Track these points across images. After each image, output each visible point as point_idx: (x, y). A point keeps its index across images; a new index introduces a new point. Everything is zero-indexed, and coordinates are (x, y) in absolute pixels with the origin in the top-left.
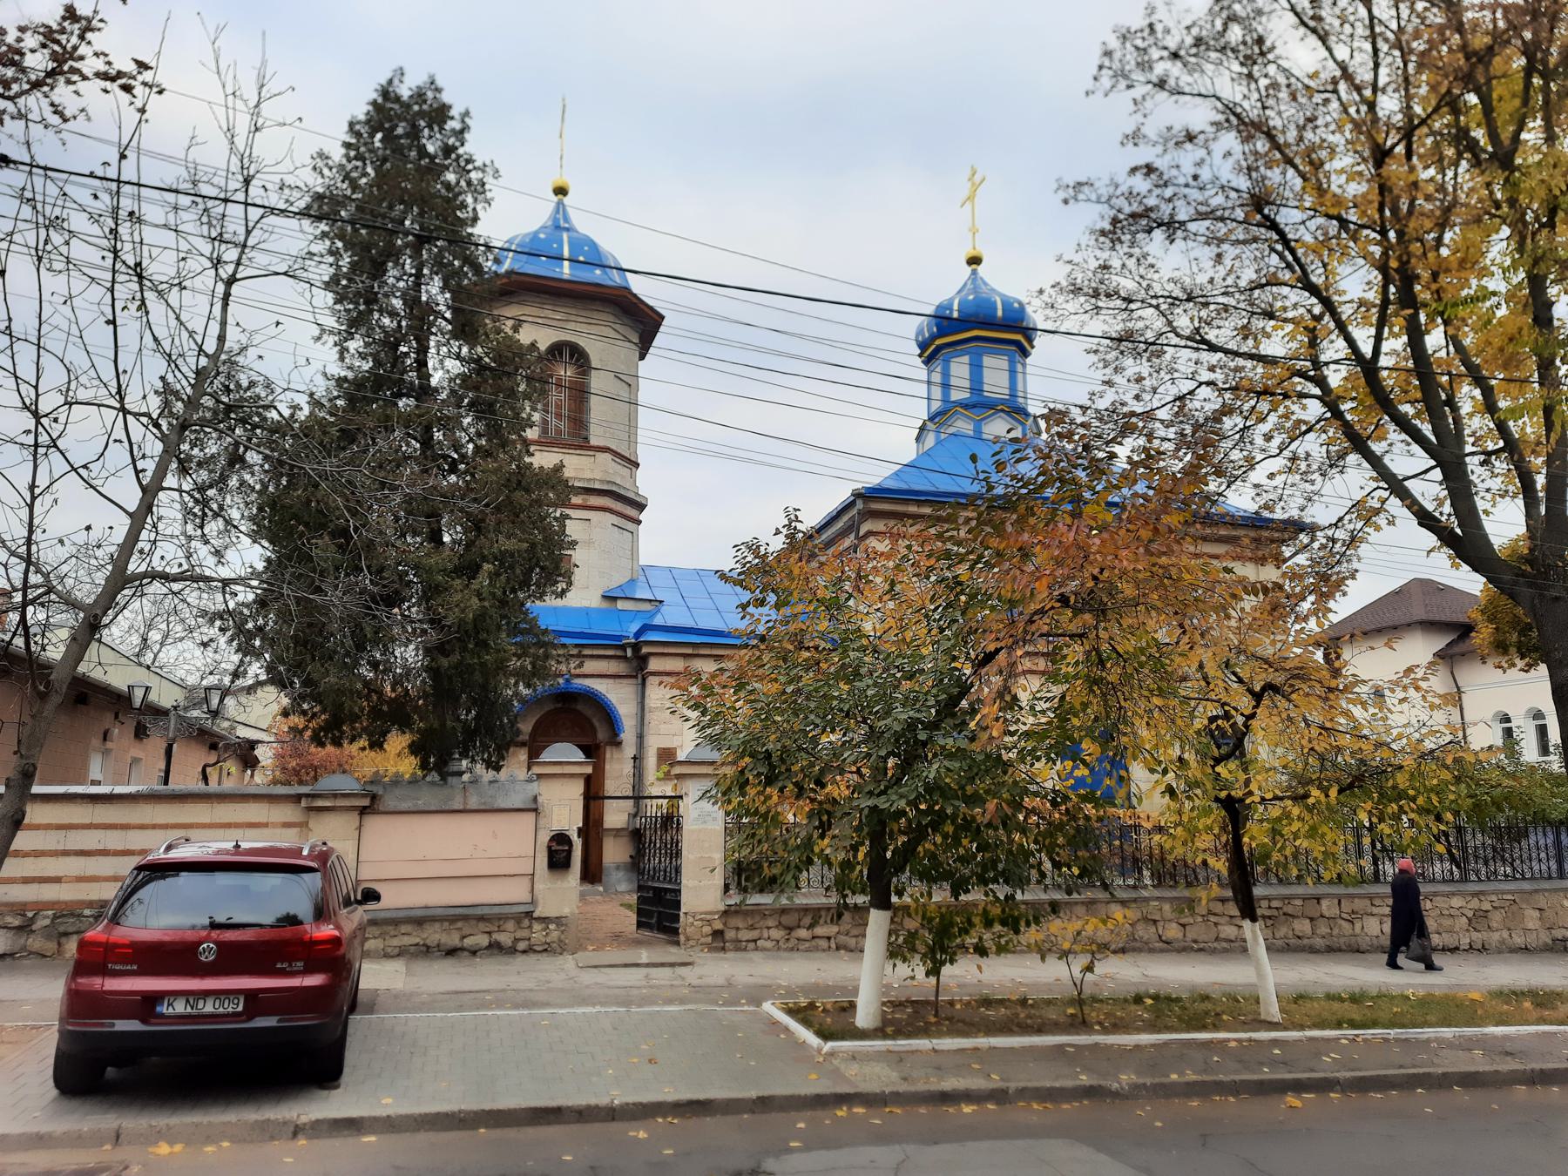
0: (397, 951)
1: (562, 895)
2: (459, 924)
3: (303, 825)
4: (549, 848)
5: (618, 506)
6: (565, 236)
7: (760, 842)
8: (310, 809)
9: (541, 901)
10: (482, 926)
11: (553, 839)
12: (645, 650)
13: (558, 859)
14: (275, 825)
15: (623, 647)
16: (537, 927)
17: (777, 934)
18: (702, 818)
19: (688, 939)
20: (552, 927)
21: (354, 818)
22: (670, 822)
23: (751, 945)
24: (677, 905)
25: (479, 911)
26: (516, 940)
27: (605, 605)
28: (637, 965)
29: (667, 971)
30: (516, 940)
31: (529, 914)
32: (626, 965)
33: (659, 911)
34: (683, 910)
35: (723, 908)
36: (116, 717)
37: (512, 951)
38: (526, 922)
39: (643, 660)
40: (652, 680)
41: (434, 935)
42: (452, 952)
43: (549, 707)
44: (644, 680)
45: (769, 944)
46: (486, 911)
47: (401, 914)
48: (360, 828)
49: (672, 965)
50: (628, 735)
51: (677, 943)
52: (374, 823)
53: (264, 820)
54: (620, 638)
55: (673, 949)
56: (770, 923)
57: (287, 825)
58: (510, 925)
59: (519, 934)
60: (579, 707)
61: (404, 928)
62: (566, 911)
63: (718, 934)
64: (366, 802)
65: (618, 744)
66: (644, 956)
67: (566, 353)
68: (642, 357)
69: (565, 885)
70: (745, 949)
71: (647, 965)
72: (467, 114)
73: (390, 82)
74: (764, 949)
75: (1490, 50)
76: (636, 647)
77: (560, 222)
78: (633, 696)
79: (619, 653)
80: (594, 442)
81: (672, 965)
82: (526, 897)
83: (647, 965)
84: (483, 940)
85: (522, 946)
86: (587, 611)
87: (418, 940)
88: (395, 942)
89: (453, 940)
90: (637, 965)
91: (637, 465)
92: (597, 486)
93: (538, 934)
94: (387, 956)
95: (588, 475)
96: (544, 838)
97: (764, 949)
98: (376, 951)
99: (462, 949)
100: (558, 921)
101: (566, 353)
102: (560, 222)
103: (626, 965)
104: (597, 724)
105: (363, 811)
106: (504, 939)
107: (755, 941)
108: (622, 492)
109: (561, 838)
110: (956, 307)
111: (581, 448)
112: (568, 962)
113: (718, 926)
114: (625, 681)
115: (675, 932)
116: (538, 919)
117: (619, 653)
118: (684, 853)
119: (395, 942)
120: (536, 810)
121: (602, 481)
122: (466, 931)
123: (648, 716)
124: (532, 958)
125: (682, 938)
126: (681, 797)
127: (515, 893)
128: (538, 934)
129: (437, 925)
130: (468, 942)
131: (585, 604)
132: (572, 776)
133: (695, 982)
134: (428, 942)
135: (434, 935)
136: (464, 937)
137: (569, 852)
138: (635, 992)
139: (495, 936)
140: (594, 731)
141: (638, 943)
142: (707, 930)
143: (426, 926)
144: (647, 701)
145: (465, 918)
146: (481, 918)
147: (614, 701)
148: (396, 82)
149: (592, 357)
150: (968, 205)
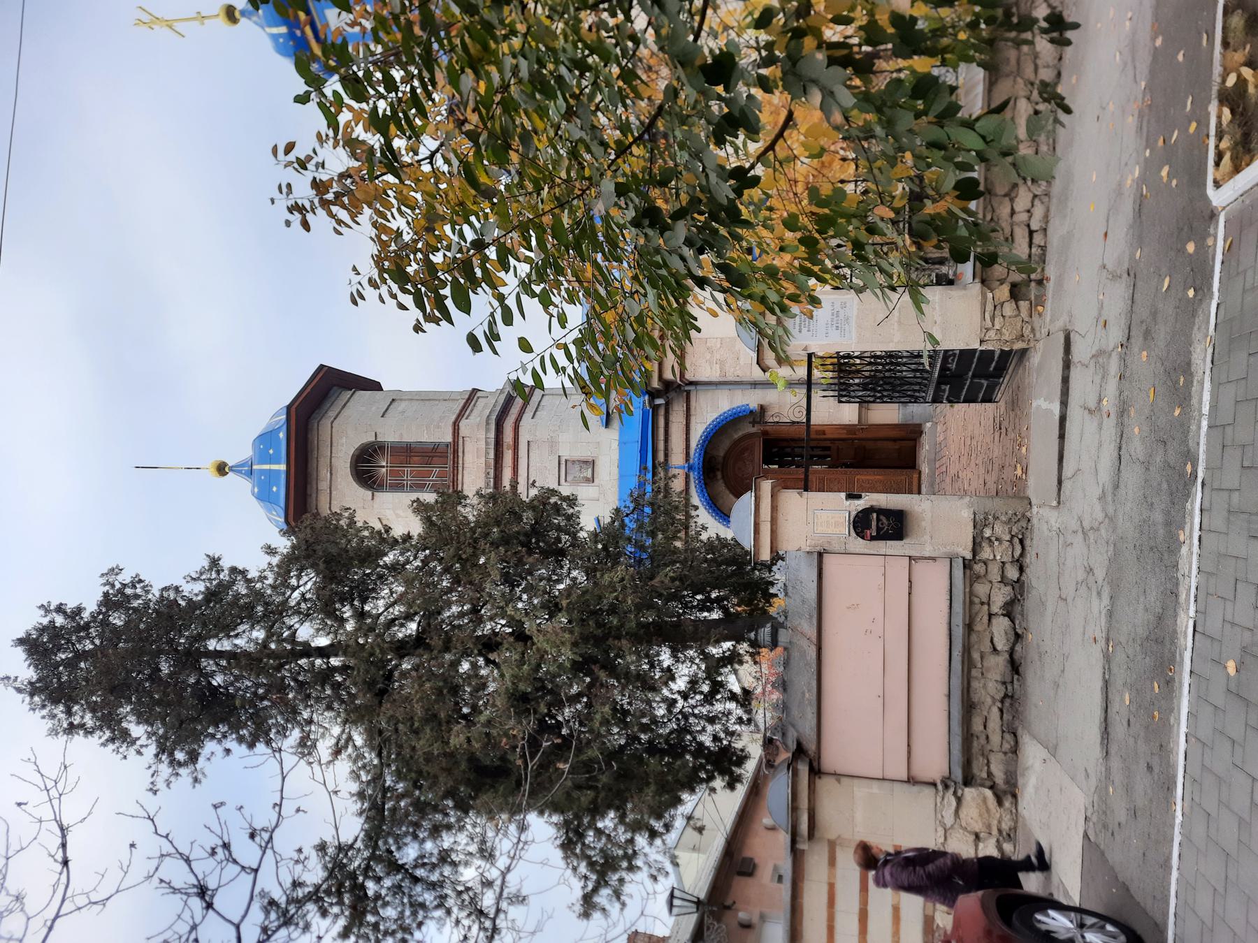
0: (1008, 737)
1: (943, 520)
2: (976, 656)
3: (832, 845)
4: (873, 538)
5: (514, 411)
6: (255, 467)
7: (872, 230)
8: (811, 835)
9: (949, 549)
10: (980, 626)
11: (861, 534)
12: (655, 384)
13: (887, 526)
14: (832, 875)
15: (655, 409)
16: (986, 553)
17: (1023, 200)
18: (838, 323)
19: (1021, 337)
20: (988, 533)
21: (824, 784)
22: (843, 366)
23: (1038, 239)
24: (966, 354)
25: (959, 632)
26: (1003, 580)
27: (616, 423)
28: (1063, 419)
29: (1075, 374)
30: (1003, 580)
31: (967, 565)
32: (1062, 436)
33: (973, 375)
34: (975, 345)
35: (977, 286)
36: (729, 908)
37: (1019, 587)
38: (979, 568)
39: (668, 386)
40: (689, 376)
41: (989, 688)
42: (1015, 666)
43: (721, 487)
44: (691, 383)
45: (1038, 211)
46: (959, 620)
47: (957, 729)
48: (838, 776)
49: (1067, 365)
50: (752, 400)
51: (1023, 353)
52: (832, 758)
53: (825, 889)
54: (645, 413)
55: (1035, 359)
56: (1005, 211)
57: (832, 862)
58: (981, 589)
59: (995, 574)
60: (722, 453)
61: (977, 726)
62: (966, 515)
63: (1016, 293)
64: (803, 769)
65: (763, 409)
66: (1044, 405)
67: (364, 466)
68: (375, 386)
69: (928, 516)
70: (1043, 248)
71: (1064, 403)
72: (45, 609)
73: (19, 690)
74: (1046, 218)
75: (855, 216)
76: (653, 394)
77: (246, 470)
78: (710, 394)
79: (662, 412)
80: (449, 439)
81: (1067, 365)
82: (942, 569)
83: (1064, 403)
84: (1001, 626)
85: (1012, 573)
86: (622, 444)
87: (995, 710)
88: (996, 738)
89: (997, 666)
90: (1063, 419)
91: (475, 391)
92: (492, 435)
93: (997, 553)
94: (1015, 750)
95: (482, 444)
96: (859, 544)
97: (1046, 218)
98: (1007, 763)
99: (1011, 653)
100: (979, 525)
101: (364, 466)
102: (246, 470)
103: (1062, 436)
104: (740, 434)
105: (816, 771)
106: (1000, 596)
107: (1031, 233)
108: (498, 408)
109: (861, 524)
110: (275, 30)
111: (456, 452)
112: (1045, 519)
113: (1004, 292)
114: (693, 403)
115: (1006, 356)
116: (975, 552)
117: (662, 412)
118: (891, 347)
119: (996, 738)
120: (820, 555)
121: (487, 430)
122: (987, 647)
123: (730, 378)
124: (1029, 559)
125: (1019, 346)
126: (810, 356)
127: (934, 587)
128: (997, 553)
129: (975, 684)
130: (1001, 644)
131: (615, 445)
132: (774, 508)
133: (1116, 334)
134: (999, 696)
135: (989, 688)
136: (995, 649)
137: (881, 512)
138: (1136, 447)
139: (996, 608)
140: (749, 436)
141: (1015, 404)
142: (1009, 309)
143: (975, 698)
144: (714, 379)
145: (967, 650)
146: (969, 627)
147: (715, 415)
148: (18, 684)
149: (364, 441)
150: (179, 26)
